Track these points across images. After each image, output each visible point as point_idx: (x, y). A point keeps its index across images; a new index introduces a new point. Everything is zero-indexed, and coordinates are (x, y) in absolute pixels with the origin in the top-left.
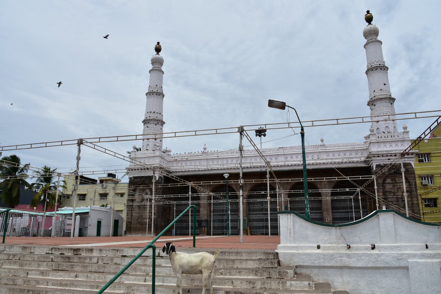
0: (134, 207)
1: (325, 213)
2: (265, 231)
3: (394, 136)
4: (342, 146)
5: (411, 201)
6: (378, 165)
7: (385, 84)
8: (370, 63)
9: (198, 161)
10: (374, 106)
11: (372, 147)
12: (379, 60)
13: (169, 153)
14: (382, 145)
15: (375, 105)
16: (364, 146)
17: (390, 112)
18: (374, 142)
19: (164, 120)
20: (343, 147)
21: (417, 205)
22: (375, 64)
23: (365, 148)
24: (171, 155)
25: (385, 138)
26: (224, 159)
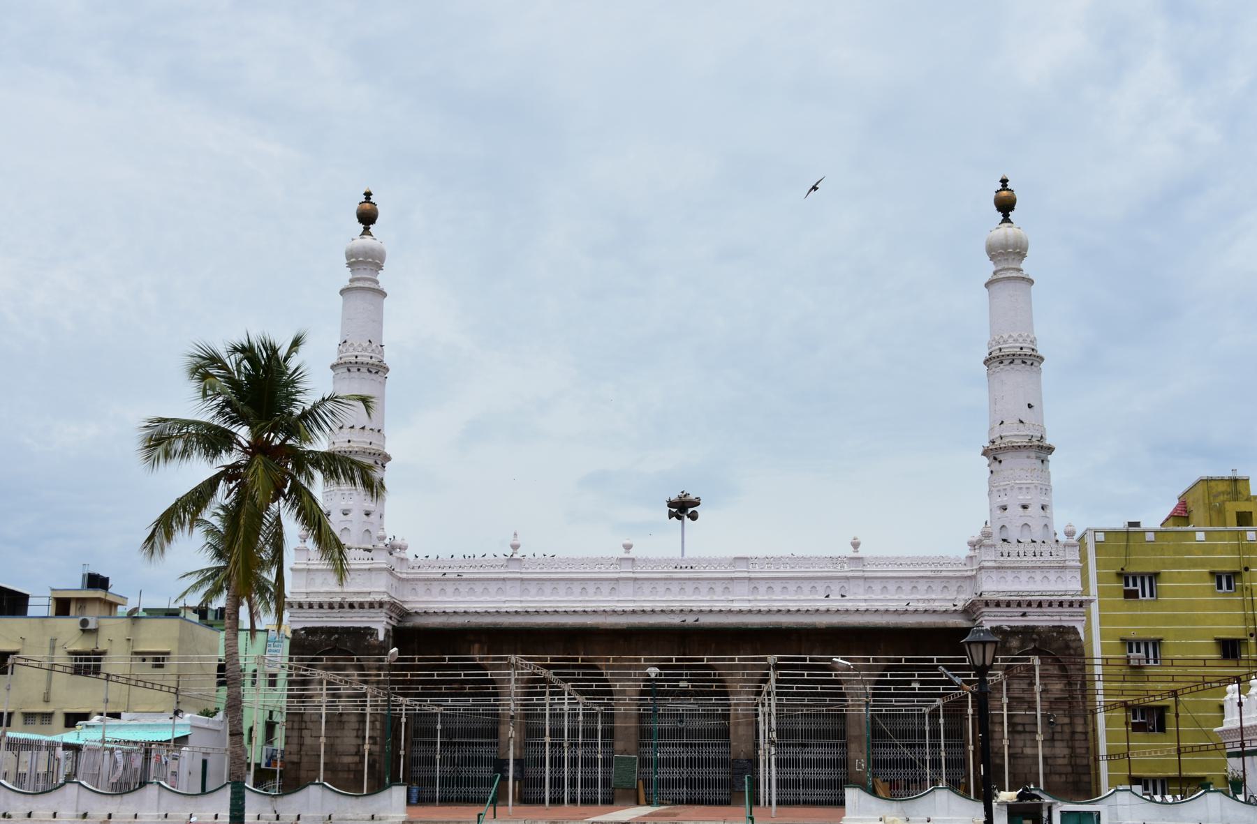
0: (306, 718)
1: (853, 747)
2: (687, 794)
3: (1041, 553)
4: (909, 563)
5: (1069, 726)
6: (997, 627)
7: (1030, 406)
8: (997, 338)
9: (809, 581)
10: (997, 463)
11: (984, 579)
12: (1020, 336)
13: (402, 555)
14: (1009, 575)
15: (1000, 462)
16: (966, 569)
17: (1036, 486)
18: (989, 568)
19: (387, 450)
20: (911, 568)
21: (1083, 737)
22: (1010, 347)
23: (969, 573)
24: (407, 560)
25: (1019, 556)
26: (575, 583)
